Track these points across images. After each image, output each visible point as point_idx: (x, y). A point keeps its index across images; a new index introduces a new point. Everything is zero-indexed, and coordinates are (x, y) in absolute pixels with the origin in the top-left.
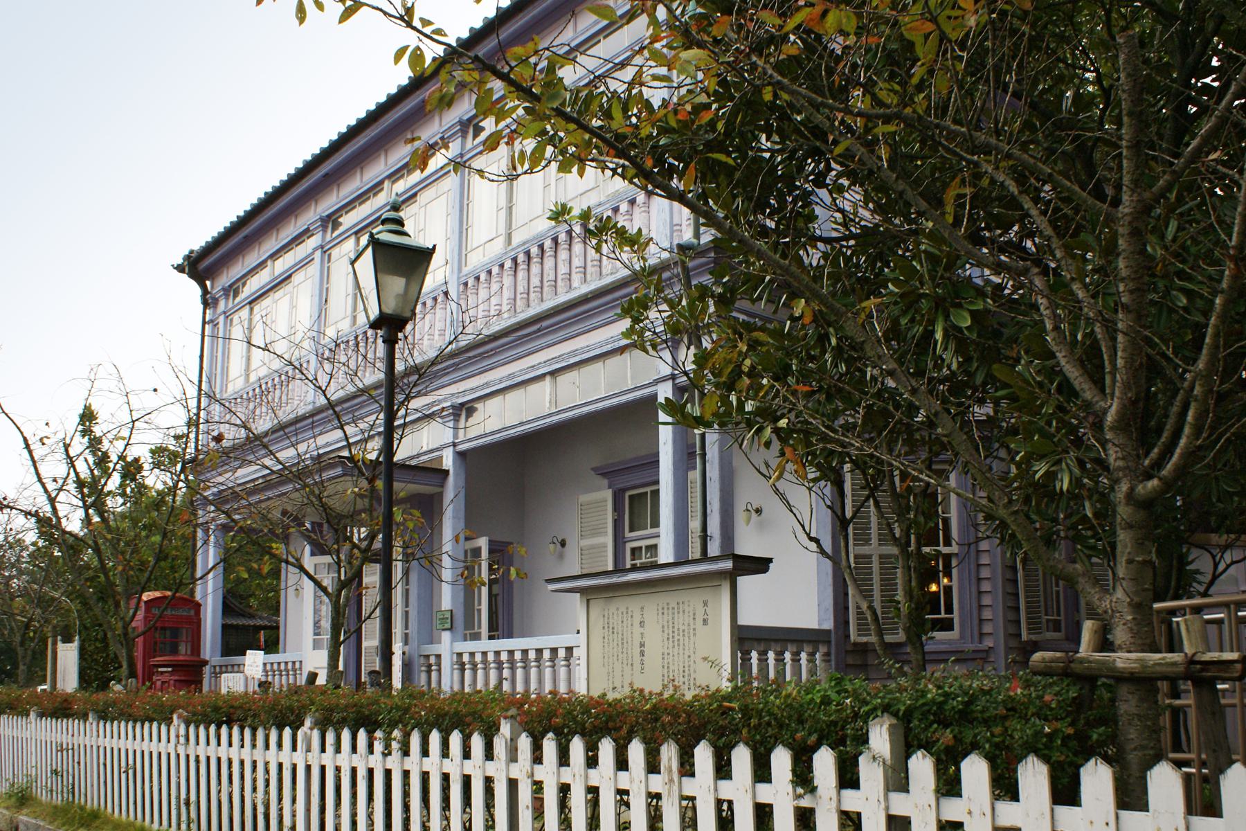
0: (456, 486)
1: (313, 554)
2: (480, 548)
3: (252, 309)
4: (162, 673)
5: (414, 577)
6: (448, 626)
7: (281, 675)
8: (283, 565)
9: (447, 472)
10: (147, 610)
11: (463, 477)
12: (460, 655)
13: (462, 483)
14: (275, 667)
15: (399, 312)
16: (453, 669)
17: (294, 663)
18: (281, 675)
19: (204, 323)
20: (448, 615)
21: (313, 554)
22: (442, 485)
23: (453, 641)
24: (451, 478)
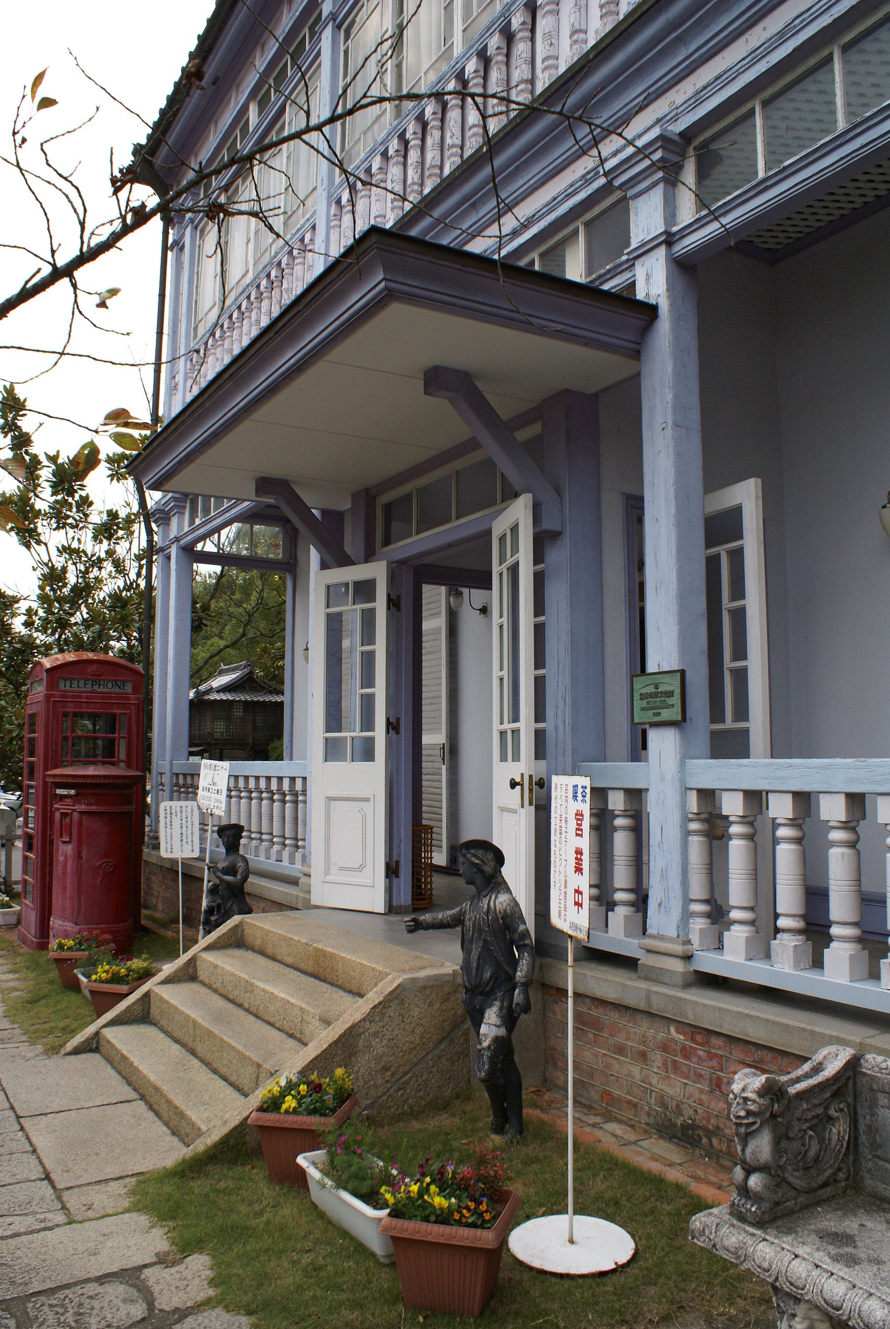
0: (678, 351)
1: (324, 566)
2: (737, 511)
3: (42, 1180)
4: (62, 797)
5: (558, 594)
6: (674, 714)
7: (284, 802)
8: (492, 143)
9: (650, 311)
10: (52, 685)
11: (692, 323)
12: (708, 796)
13: (691, 340)
14: (263, 784)
15: (420, 237)
16: (687, 833)
17: (293, 779)
18: (284, 802)
19: (165, 249)
20: (674, 685)
21: (324, 566)
22: (636, 352)
23: (685, 756)
24: (664, 326)
